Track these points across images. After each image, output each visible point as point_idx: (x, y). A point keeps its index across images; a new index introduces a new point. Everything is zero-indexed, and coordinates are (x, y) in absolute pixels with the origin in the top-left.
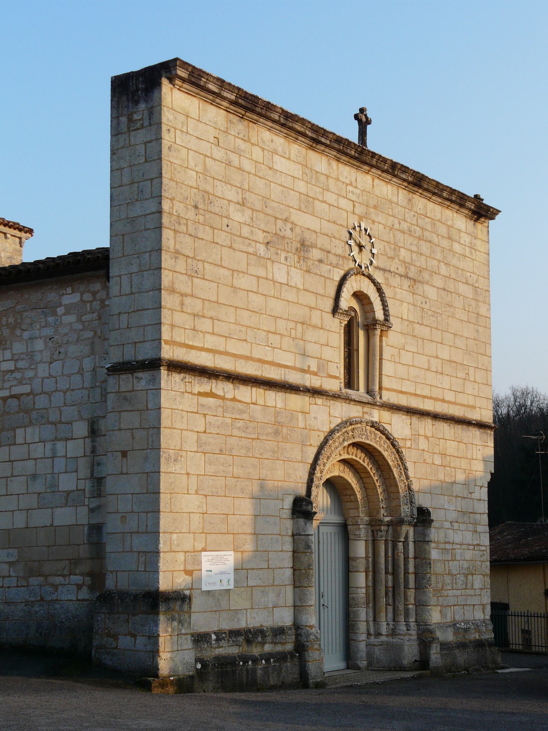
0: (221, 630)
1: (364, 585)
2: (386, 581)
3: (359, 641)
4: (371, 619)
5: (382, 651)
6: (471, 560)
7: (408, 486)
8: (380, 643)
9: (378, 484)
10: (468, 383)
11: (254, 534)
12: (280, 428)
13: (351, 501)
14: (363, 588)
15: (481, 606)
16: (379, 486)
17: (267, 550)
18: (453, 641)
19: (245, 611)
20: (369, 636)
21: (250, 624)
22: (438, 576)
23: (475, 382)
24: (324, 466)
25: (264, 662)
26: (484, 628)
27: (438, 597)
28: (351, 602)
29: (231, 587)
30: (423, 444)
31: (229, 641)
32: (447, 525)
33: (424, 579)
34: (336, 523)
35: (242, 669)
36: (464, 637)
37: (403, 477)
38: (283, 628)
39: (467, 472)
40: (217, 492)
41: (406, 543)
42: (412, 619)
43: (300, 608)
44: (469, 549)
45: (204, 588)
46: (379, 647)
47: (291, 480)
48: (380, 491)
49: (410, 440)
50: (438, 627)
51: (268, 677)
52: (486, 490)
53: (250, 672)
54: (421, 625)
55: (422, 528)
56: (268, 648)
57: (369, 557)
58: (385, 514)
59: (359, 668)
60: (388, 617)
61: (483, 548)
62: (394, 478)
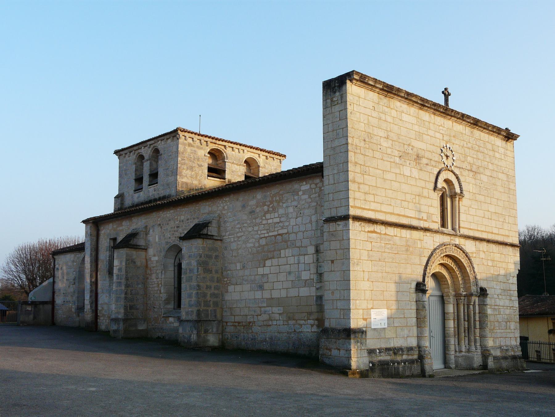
1: (453, 327)
2: (464, 325)
4: (457, 344)
9: (459, 276)
14: (452, 328)
15: (515, 338)
25: (403, 364)
28: (446, 335)
29: (386, 326)
30: (482, 255)
32: (496, 296)
35: (392, 367)
37: (472, 272)
39: (506, 269)
40: (378, 280)
41: (474, 305)
42: (478, 344)
43: (421, 338)
45: (373, 327)
48: (460, 279)
49: (476, 253)
55: (483, 298)
56: (405, 357)
59: (451, 368)
60: (466, 343)
61: (515, 308)
62: (468, 273)
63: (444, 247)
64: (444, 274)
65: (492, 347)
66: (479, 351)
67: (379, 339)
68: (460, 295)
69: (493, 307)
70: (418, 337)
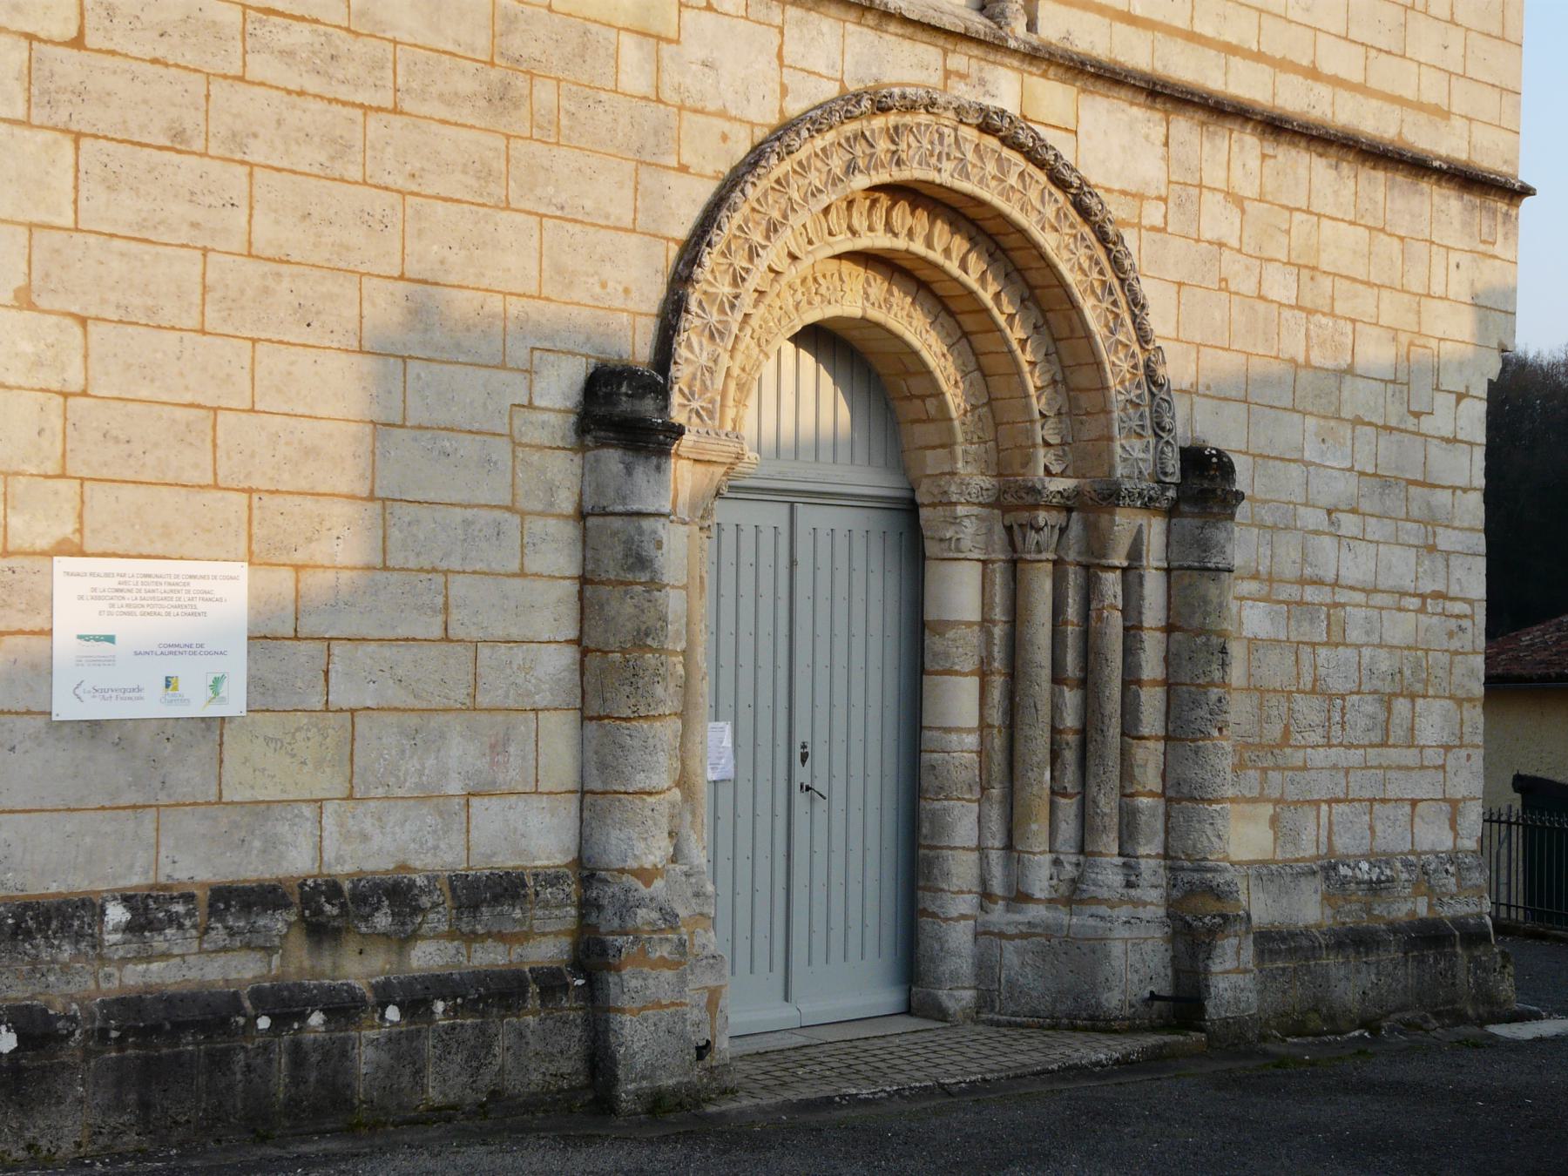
0: (165, 888)
1: (974, 722)
2: (1056, 709)
3: (947, 920)
4: (996, 841)
5: (1028, 958)
6: (1409, 648)
7: (1147, 366)
8: (1024, 929)
9: (1024, 358)
10: (1419, 24)
11: (371, 498)
12: (521, 83)
13: (929, 420)
14: (969, 731)
15: (1445, 807)
16: (1032, 364)
17: (444, 565)
18: (1318, 926)
19: (307, 811)
20: (986, 903)
21: (340, 859)
22: (1267, 696)
23: (1452, 22)
24: (751, 260)
25: (393, 1013)
26: (1453, 880)
27: (1264, 770)
28: (927, 780)
29: (234, 703)
30: (1218, 220)
31: (207, 930)
32: (1313, 518)
33: (1196, 704)
34: (882, 497)
35: (266, 1049)
36: (1369, 911)
37: (1127, 333)
38: (520, 877)
39: (1404, 339)
40: (152, 311)
41: (1131, 573)
42: (1149, 848)
43: (600, 800)
44: (1400, 609)
45: (66, 708)
46: (1017, 941)
47: (578, 295)
48: (1032, 381)
49: (1165, 200)
50: (1260, 877)
51: (418, 1073)
52: (1481, 408)
53: (314, 1058)
54: (1182, 869)
55: (1197, 522)
56: (427, 957)
57: (993, 622)
58: (1056, 469)
59: (940, 1014)
60: (1060, 838)
61: (1459, 608)
62: (1089, 336)
63: (879, 122)
64: (910, 337)
65: (1264, 863)
66: (1154, 895)
67: (149, 816)
68: (1030, 499)
69: (1289, 592)
70: (584, 793)
